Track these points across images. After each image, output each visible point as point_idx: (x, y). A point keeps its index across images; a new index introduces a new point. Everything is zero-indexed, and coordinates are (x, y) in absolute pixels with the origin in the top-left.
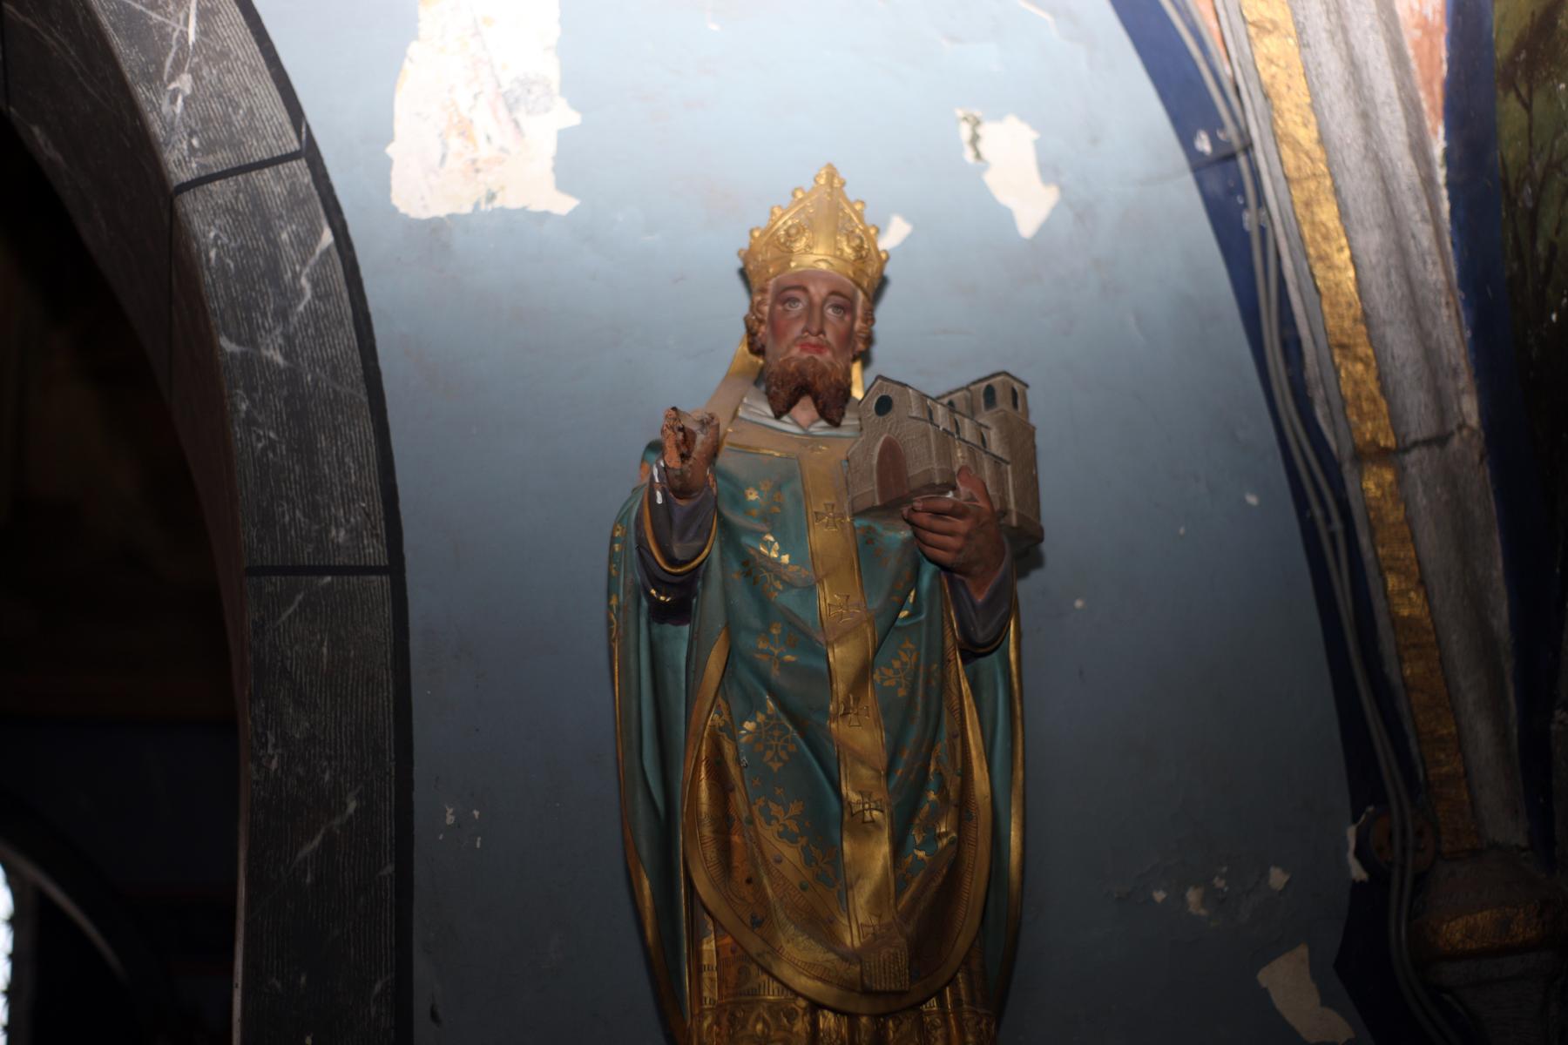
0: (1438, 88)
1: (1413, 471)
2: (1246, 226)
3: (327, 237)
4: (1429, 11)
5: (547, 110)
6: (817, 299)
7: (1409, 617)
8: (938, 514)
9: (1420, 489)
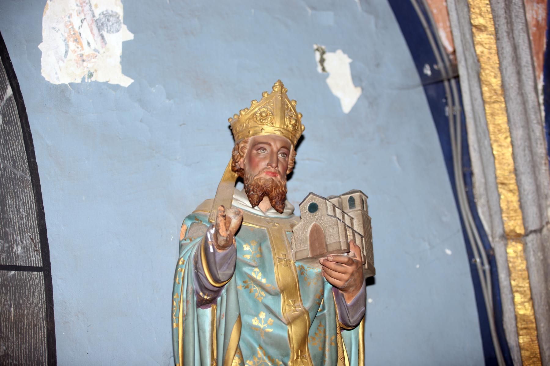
0: (541, 56)
1: (529, 245)
2: (447, 114)
3: (9, 92)
4: (540, 19)
5: (118, 31)
6: (275, 149)
7: (524, 315)
8: (339, 263)
9: (532, 253)
